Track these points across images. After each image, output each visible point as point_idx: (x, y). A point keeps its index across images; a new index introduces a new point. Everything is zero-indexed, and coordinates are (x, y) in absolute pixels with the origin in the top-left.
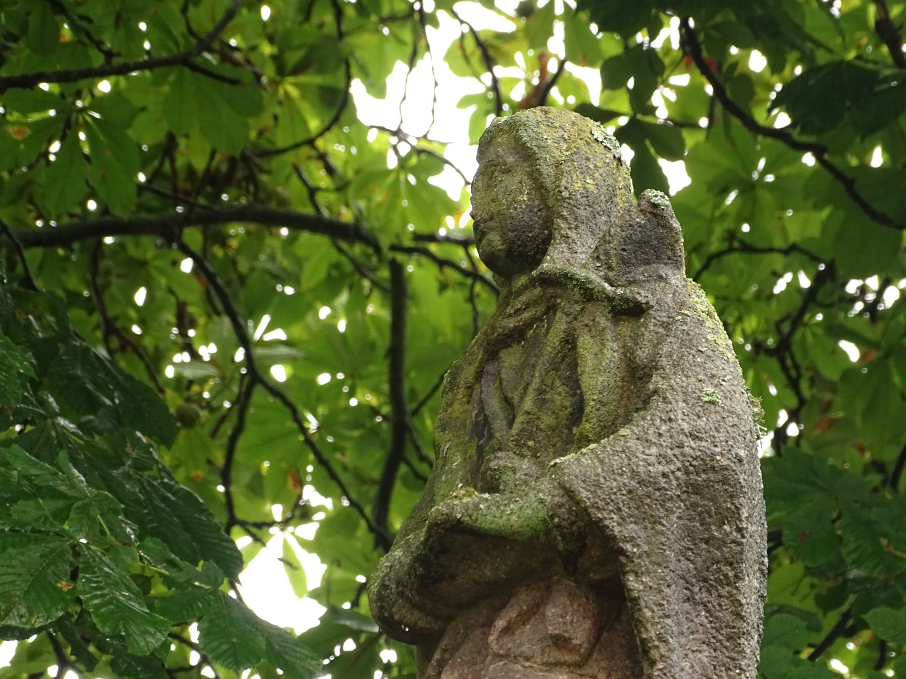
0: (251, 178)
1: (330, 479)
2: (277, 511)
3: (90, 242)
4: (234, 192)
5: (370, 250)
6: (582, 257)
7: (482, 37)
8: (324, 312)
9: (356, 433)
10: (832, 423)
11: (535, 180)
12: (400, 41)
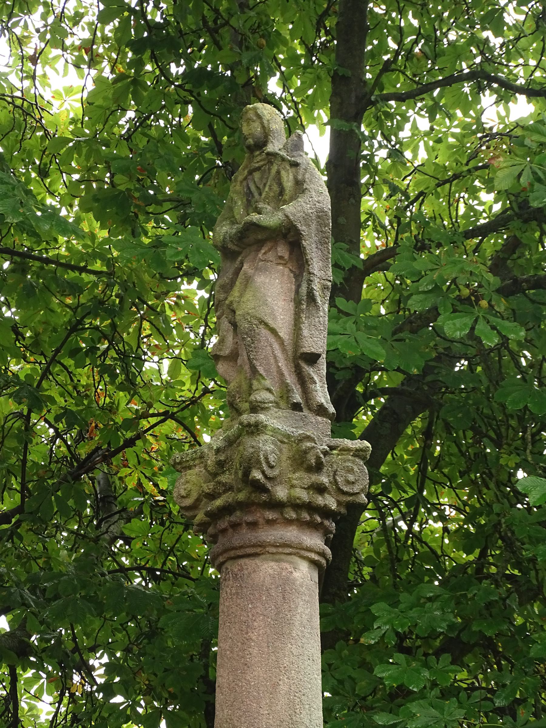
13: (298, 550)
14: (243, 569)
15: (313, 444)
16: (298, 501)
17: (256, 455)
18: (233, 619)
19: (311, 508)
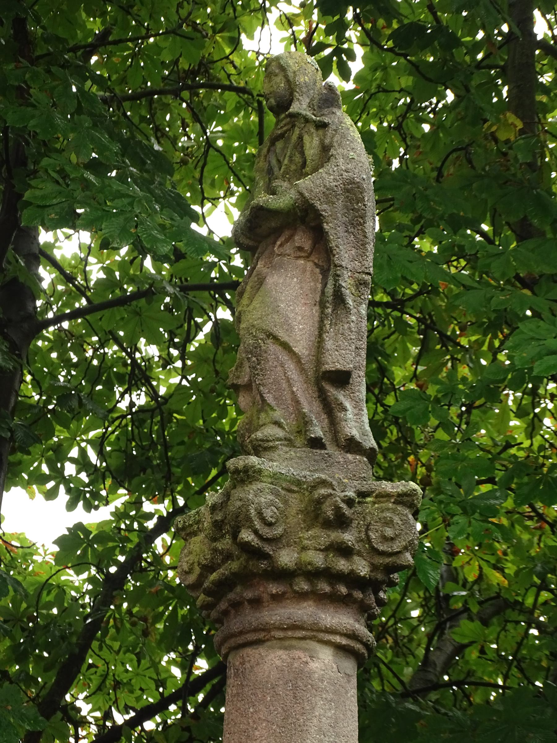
0: (207, 71)
1: (239, 181)
2: (222, 194)
3: (149, 97)
4: (201, 77)
5: (250, 97)
6: (305, 106)
7: (288, 16)
8: (236, 119)
9: (248, 164)
10: (420, 153)
11: (286, 78)
12: (258, 19)
13: (316, 633)
14: (245, 661)
15: (330, 491)
16: (309, 567)
17: (244, 510)
18: (232, 729)
19: (332, 576)
